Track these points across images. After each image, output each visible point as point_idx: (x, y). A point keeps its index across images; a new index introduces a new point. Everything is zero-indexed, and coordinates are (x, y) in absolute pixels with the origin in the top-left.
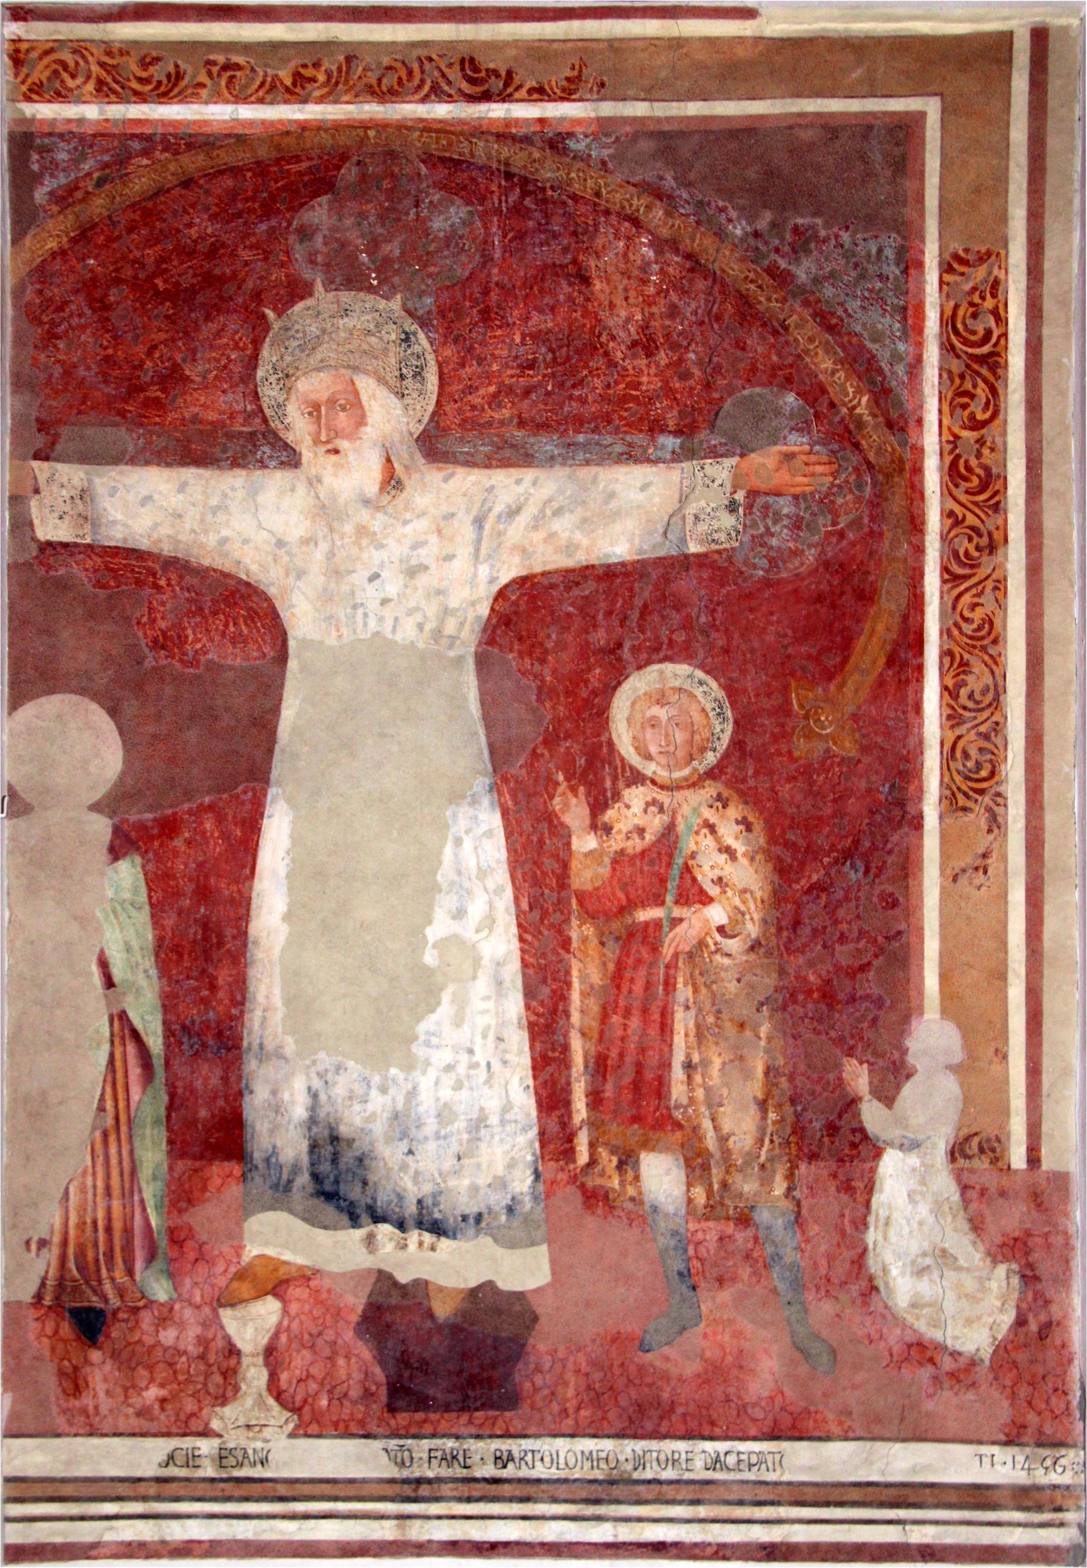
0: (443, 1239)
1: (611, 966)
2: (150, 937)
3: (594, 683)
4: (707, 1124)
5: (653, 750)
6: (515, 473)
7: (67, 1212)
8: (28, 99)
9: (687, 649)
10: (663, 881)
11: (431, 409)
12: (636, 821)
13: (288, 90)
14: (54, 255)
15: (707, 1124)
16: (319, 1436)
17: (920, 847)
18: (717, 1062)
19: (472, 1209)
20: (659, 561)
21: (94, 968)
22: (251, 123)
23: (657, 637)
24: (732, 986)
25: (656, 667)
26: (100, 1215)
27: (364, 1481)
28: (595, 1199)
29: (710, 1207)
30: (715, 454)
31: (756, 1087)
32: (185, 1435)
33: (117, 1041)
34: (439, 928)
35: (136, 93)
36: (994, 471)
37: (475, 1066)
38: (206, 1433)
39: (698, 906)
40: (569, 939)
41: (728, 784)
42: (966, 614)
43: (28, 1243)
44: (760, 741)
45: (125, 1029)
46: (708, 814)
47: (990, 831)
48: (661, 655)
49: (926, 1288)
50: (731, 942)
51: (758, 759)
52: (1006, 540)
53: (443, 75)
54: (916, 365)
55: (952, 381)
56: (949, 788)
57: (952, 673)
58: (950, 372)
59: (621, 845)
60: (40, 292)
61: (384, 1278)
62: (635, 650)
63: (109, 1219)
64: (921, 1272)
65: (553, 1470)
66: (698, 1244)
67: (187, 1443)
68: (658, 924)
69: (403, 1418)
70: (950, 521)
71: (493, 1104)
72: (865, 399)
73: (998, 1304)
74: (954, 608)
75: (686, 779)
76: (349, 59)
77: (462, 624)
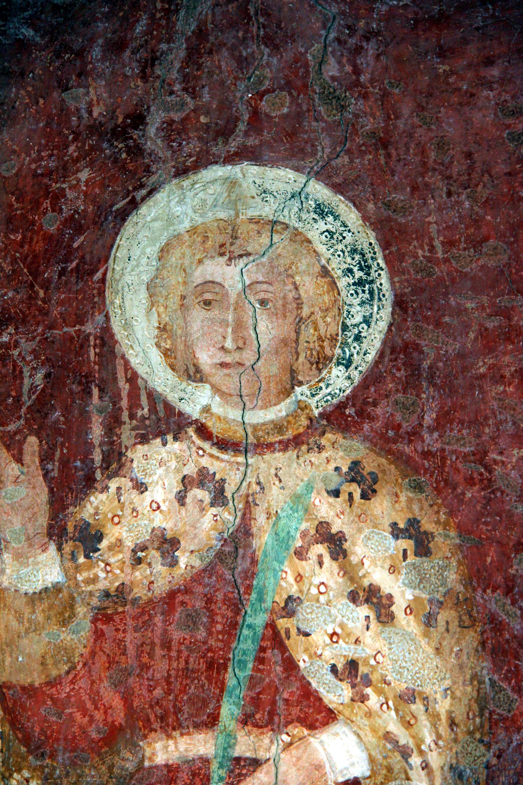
3: (75, 201)
5: (206, 358)
9: (292, 135)
10: (216, 667)
12: (159, 521)
23: (225, 105)
25: (218, 171)
39: (298, 730)
41: (384, 443)
44: (453, 347)
46: (326, 509)
48: (233, 146)
51: (448, 387)
59: (122, 576)
62: (172, 131)
75: (278, 427)
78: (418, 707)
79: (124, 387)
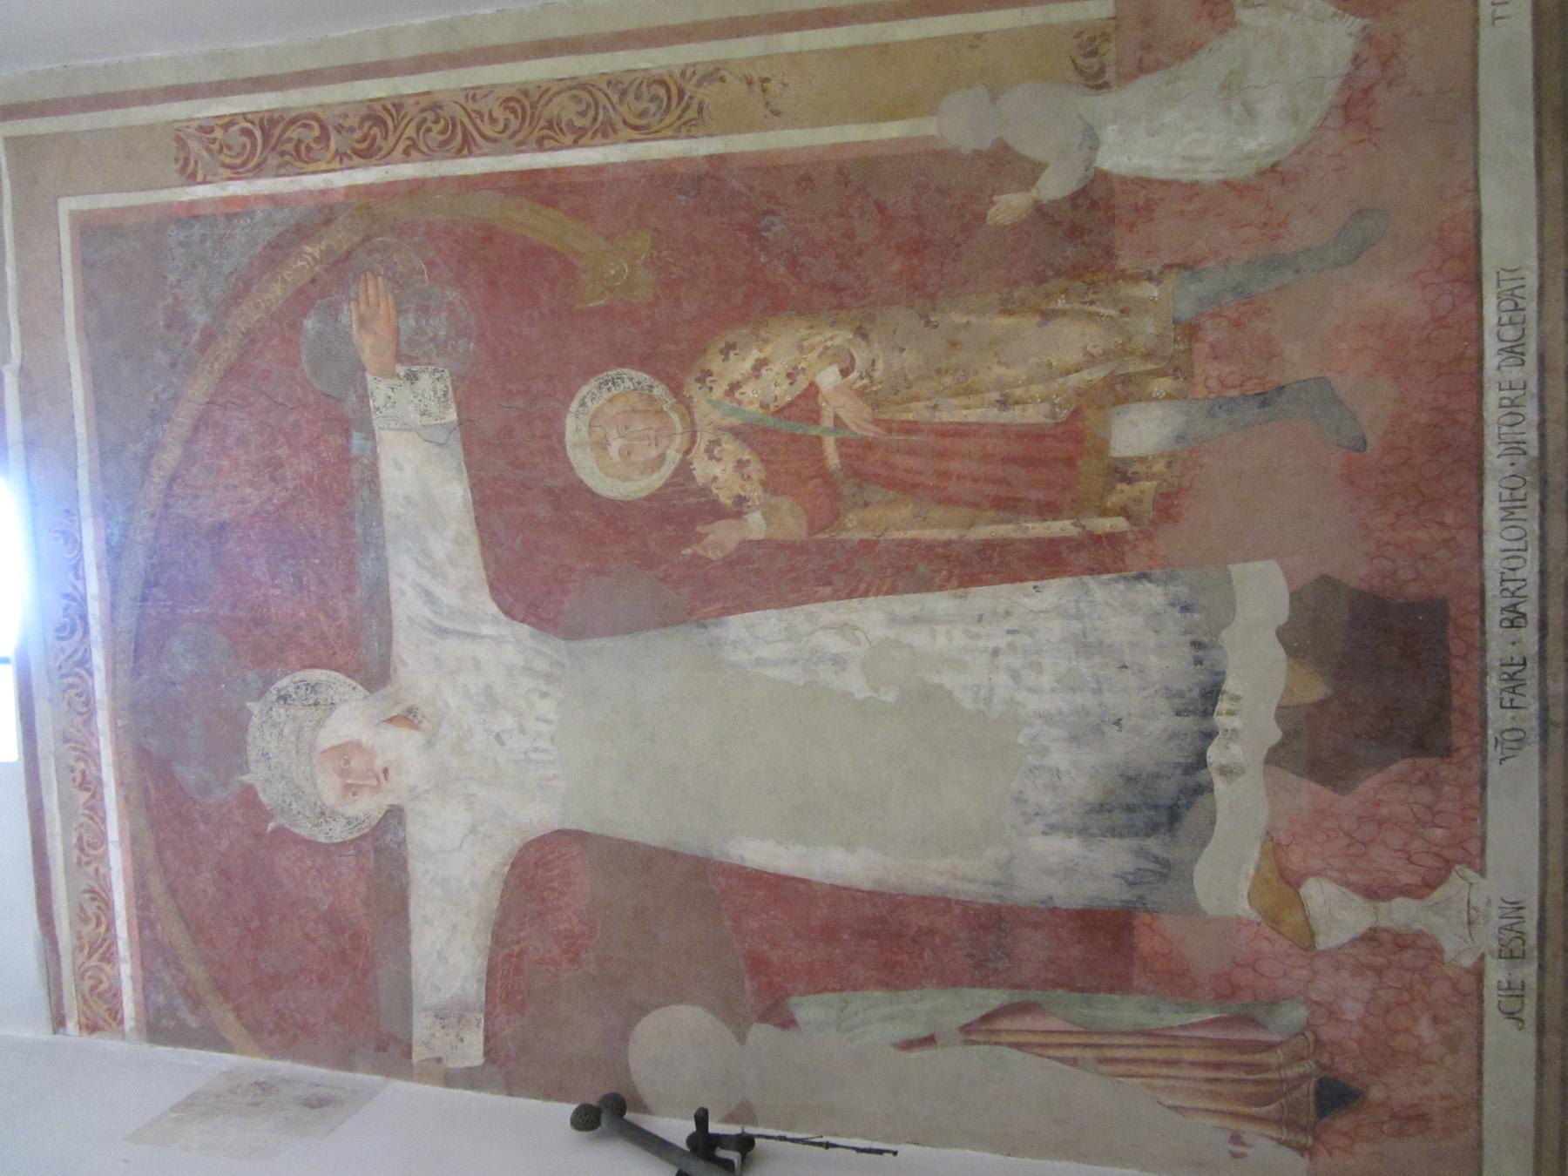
0: (1225, 687)
1: (892, 494)
2: (878, 994)
4: (1074, 380)
5: (654, 452)
6: (394, 596)
7: (1197, 1110)
8: (121, 1022)
10: (794, 439)
11: (341, 677)
13: (93, 796)
14: (239, 1017)
15: (1074, 380)
16: (1483, 839)
17: (744, 155)
18: (998, 371)
19: (1188, 652)
20: (468, 451)
21: (915, 1054)
22: (121, 832)
24: (910, 358)
25: (570, 453)
26: (1200, 1073)
27: (1544, 787)
28: (1167, 507)
29: (1176, 372)
30: (364, 398)
31: (1027, 324)
32: (1481, 998)
33: (994, 1038)
34: (854, 683)
35: (108, 930)
36: (364, 112)
37: (1011, 645)
38: (1478, 973)
40: (862, 541)
42: (501, 127)
43: (1235, 1155)
45: (981, 1028)
46: (718, 392)
47: (722, 80)
49: (1270, 107)
50: (858, 363)
52: (428, 93)
53: (69, 657)
54: (275, 200)
55: (287, 163)
56: (679, 130)
57: (560, 137)
58: (280, 166)
60: (271, 1033)
61: (1276, 757)
63: (1206, 1065)
64: (1250, 113)
65: (1528, 555)
66: (1223, 385)
67: (1491, 996)
68: (841, 443)
69: (1459, 739)
70: (414, 153)
71: (1055, 628)
72: (308, 249)
73: (1288, 15)
74: (495, 141)
75: (682, 418)
76: (66, 740)
77: (539, 652)
78: (806, 344)
79: (669, 490)
